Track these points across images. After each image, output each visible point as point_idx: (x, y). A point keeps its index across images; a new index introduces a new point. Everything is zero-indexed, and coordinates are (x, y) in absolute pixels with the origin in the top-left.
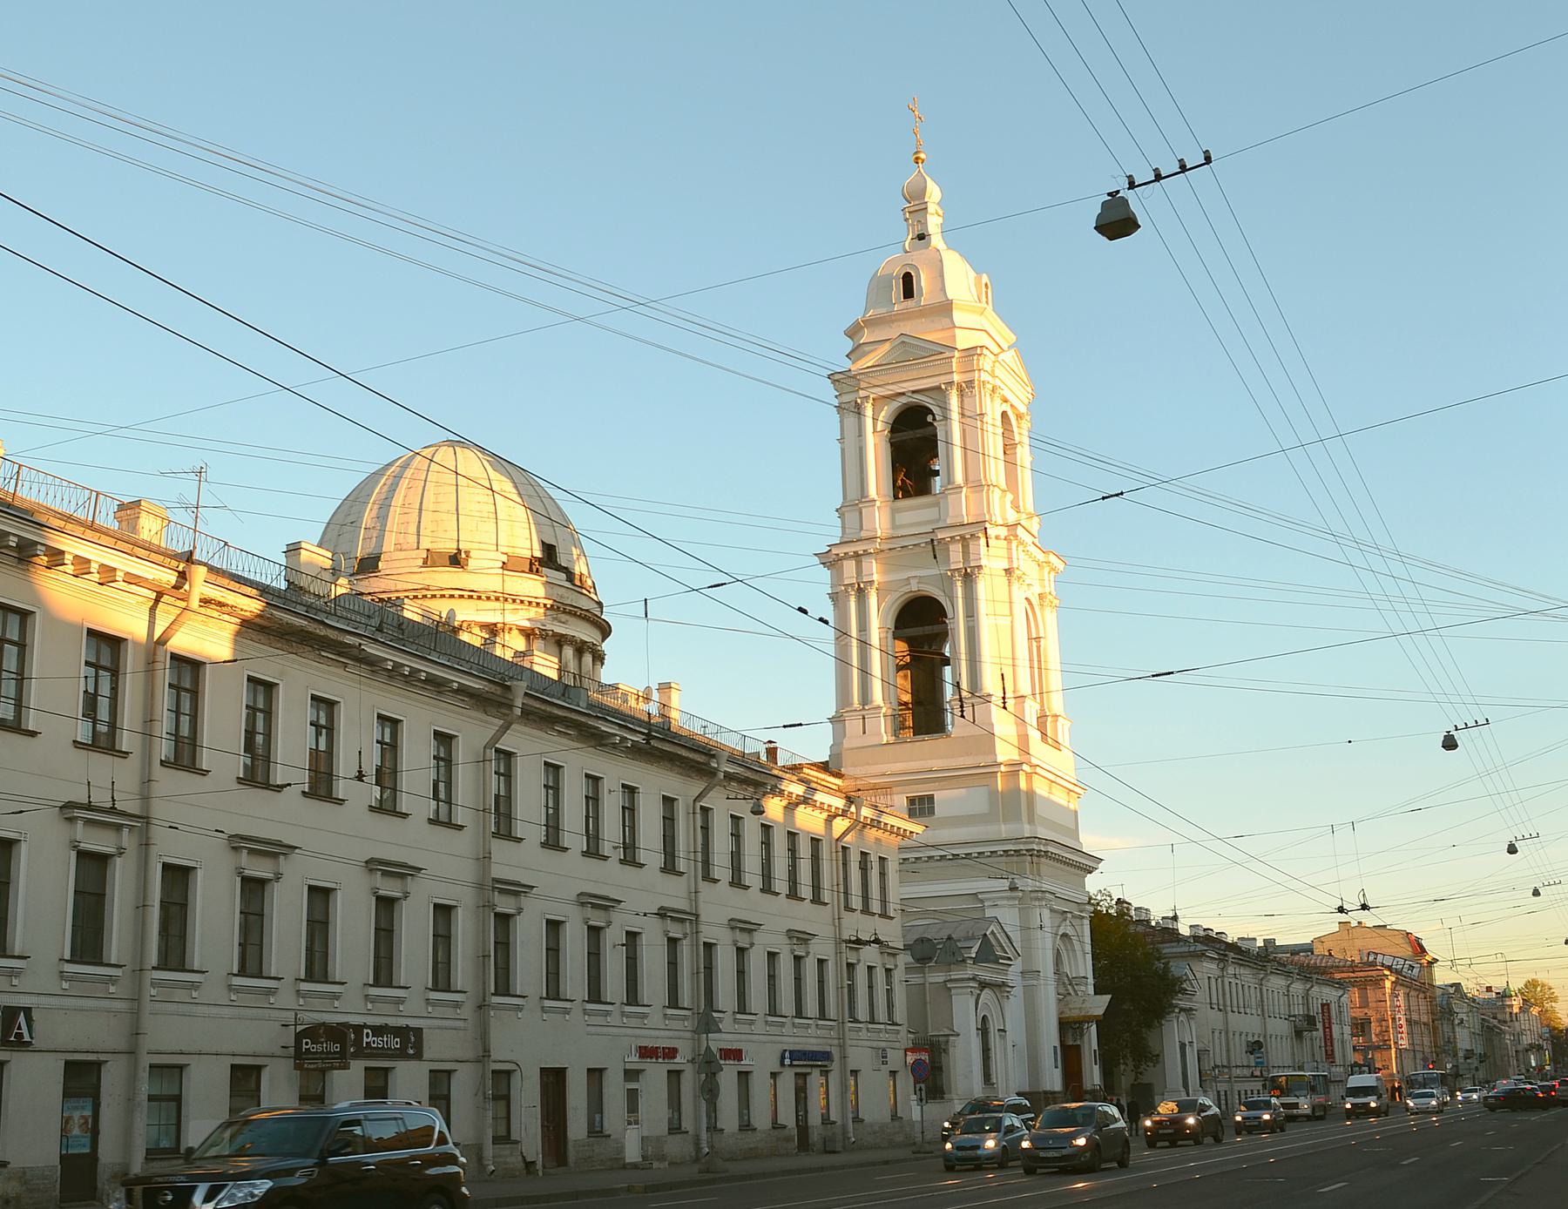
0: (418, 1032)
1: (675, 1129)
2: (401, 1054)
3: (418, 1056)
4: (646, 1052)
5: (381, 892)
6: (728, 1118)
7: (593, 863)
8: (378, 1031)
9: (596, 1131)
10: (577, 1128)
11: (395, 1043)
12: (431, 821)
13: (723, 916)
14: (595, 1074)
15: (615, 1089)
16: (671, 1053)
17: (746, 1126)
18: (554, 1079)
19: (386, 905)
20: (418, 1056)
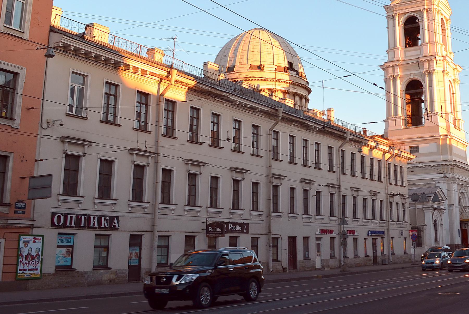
0: (247, 225)
1: (333, 257)
2: (242, 232)
3: (247, 233)
4: (323, 231)
6: (350, 253)
8: (234, 224)
9: (306, 258)
10: (300, 256)
11: (240, 228)
12: (232, 150)
14: (306, 239)
15: (312, 244)
16: (331, 232)
17: (356, 256)
19: (139, 169)
20: (247, 233)
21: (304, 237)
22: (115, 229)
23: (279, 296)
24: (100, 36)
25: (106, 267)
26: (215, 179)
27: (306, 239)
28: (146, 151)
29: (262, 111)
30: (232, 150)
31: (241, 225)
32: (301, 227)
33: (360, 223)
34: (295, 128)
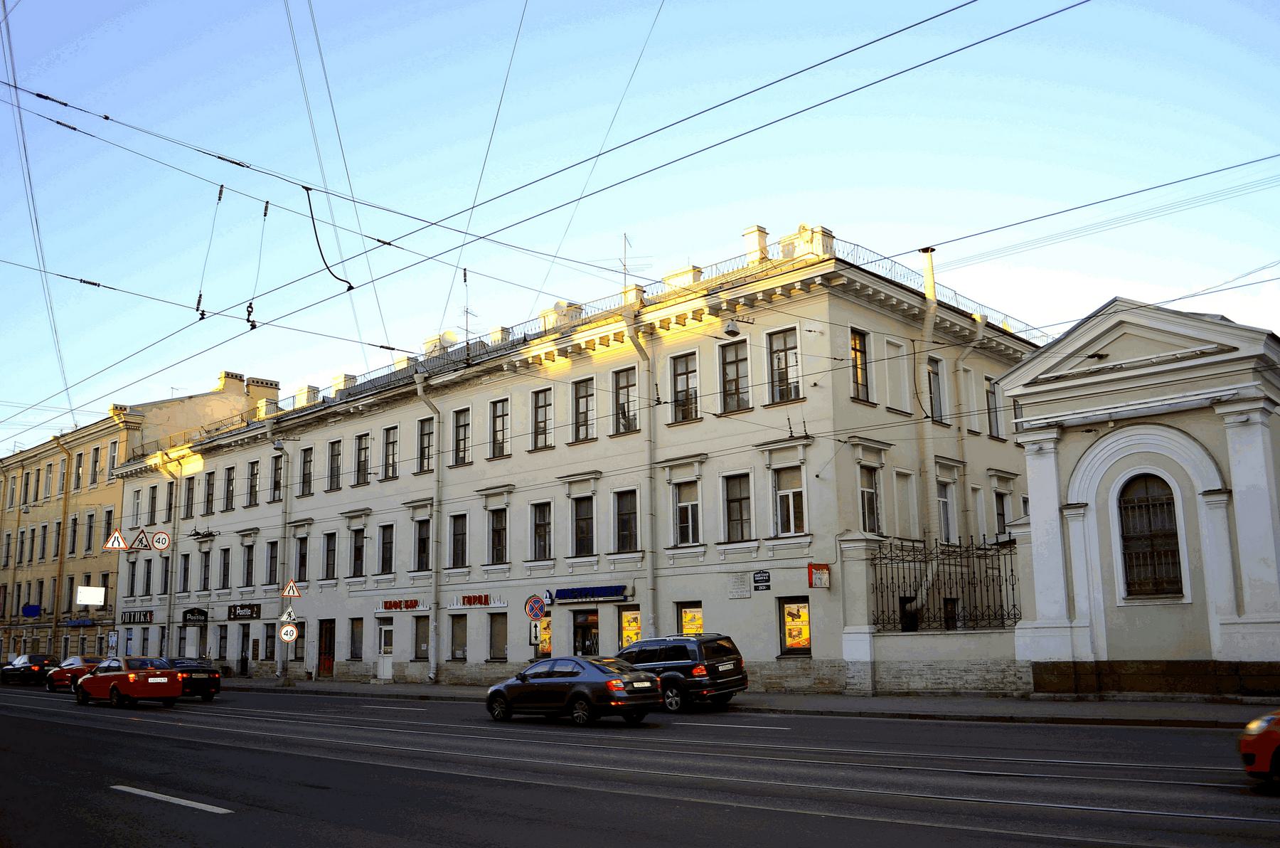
0: (259, 606)
1: (421, 657)
2: (251, 617)
3: (258, 617)
4: (469, 600)
5: (863, 463)
6: (213, 654)
7: (861, 409)
8: (242, 607)
9: (356, 655)
10: (342, 651)
11: (248, 612)
12: (489, 460)
13: (335, 512)
14: (356, 622)
15: (370, 633)
16: (412, 604)
17: (498, 657)
18: (327, 627)
19: (498, 515)
20: (258, 617)
21: (333, 621)
22: (150, 622)
23: (766, 749)
24: (458, 339)
25: (503, 660)
26: (387, 529)
27: (356, 622)
28: (792, 438)
29: (370, 407)
30: (489, 460)
31: (250, 607)
32: (348, 601)
33: (342, 587)
34: (338, 425)
